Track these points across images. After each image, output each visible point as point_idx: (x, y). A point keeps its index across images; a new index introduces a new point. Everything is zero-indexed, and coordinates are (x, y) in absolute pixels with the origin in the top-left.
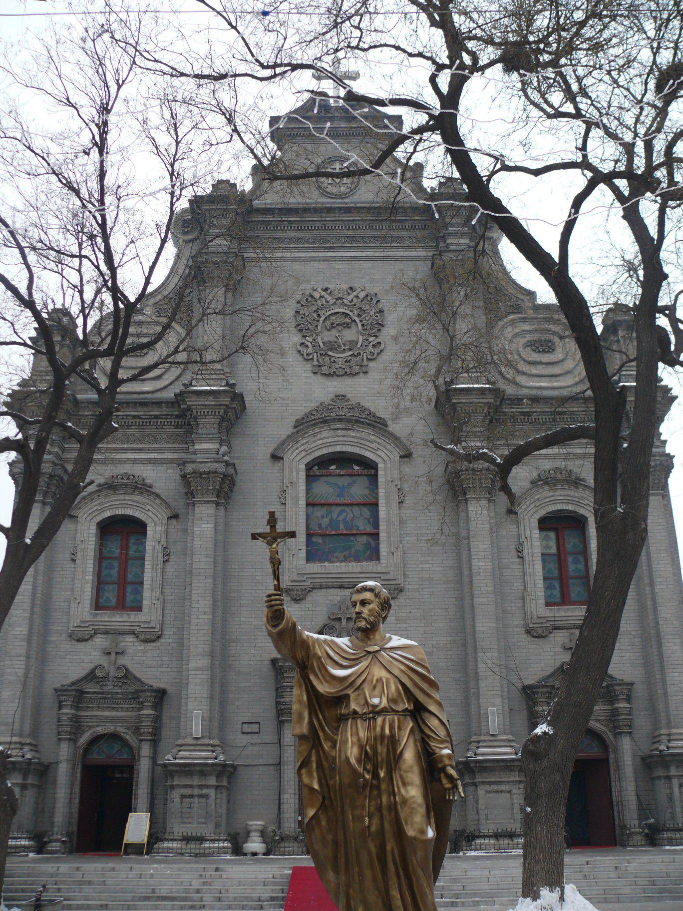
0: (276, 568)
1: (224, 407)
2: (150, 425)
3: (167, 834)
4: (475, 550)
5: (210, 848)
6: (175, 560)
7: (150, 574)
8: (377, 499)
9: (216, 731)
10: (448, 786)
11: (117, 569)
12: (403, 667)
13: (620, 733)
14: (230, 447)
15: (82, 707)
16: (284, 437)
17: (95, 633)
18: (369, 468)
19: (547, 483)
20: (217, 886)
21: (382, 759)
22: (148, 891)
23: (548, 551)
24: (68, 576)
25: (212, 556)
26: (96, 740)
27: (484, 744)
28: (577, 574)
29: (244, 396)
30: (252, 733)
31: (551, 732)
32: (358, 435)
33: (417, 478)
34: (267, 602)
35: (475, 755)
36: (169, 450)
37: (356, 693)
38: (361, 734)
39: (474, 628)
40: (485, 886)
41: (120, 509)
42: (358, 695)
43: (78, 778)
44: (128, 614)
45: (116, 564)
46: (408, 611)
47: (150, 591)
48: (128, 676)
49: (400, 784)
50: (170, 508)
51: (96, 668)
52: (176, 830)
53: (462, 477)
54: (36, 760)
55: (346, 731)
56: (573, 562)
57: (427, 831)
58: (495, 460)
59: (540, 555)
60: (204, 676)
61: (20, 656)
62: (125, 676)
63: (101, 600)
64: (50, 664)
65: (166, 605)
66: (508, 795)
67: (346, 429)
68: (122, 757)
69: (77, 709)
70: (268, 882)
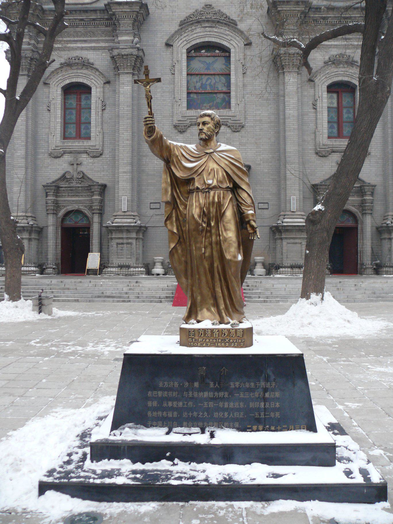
0: (149, 101)
1: (136, 13)
2: (90, 25)
3: (110, 264)
4: (288, 103)
5: (133, 271)
6: (109, 109)
7: (94, 117)
8: (230, 71)
9: (135, 208)
10: (251, 231)
11: (75, 115)
12: (227, 162)
13: (366, 213)
14: (140, 38)
15: (60, 196)
16: (173, 32)
17: (64, 153)
18: (225, 51)
19: (334, 63)
20: (137, 290)
21: (213, 217)
22: (99, 293)
23: (332, 106)
24: (46, 120)
25: (131, 106)
26: (68, 214)
27: (288, 217)
28: (348, 120)
29: (148, 5)
30: (156, 209)
31: (323, 209)
32: (219, 31)
33: (252, 57)
34: (144, 122)
35: (282, 222)
36: (103, 41)
37: (199, 177)
38: (201, 201)
39: (285, 150)
40: (283, 293)
41: (75, 79)
42: (200, 178)
43: (60, 235)
44: (83, 141)
45: (74, 112)
46: (247, 139)
47: (95, 127)
48: (84, 177)
49: (223, 230)
50: (105, 77)
51: (66, 173)
52: (114, 262)
53: (282, 58)
54: (35, 225)
55: (192, 199)
56: (346, 113)
57: (238, 257)
58: (300, 46)
59: (326, 107)
60: (128, 176)
61: (22, 167)
62: (83, 177)
63: (67, 134)
64: (40, 171)
65: (105, 135)
66: (299, 245)
67: (211, 27)
68: (83, 223)
69: (57, 196)
70: (164, 289)
